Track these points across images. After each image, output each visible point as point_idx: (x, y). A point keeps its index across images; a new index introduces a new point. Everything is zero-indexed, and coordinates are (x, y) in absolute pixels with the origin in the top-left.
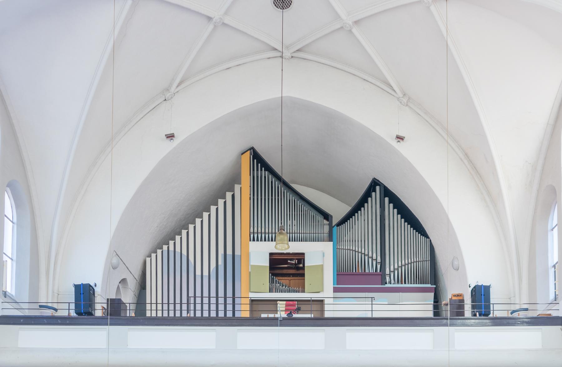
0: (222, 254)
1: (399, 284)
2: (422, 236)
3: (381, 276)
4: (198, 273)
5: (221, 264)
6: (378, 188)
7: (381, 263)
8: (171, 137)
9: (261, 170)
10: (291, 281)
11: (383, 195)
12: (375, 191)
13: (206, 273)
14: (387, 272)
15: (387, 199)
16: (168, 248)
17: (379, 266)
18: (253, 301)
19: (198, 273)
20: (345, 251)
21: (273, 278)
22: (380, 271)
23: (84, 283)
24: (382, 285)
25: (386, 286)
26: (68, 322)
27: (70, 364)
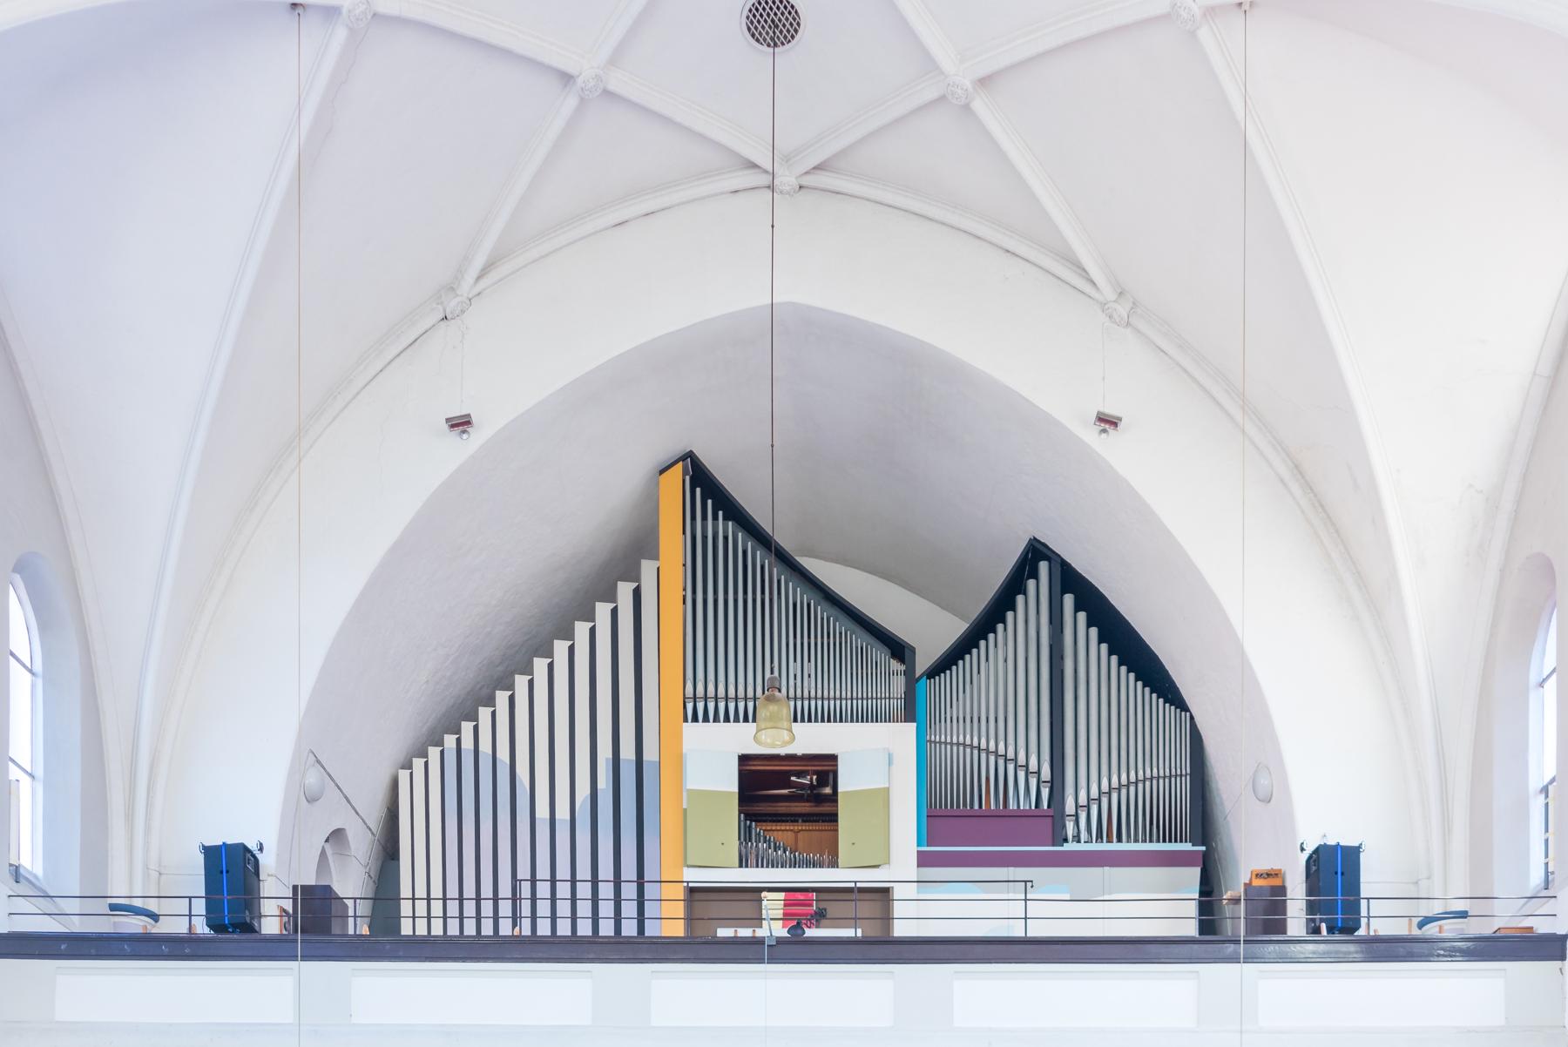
0: (607, 759)
1: (1102, 842)
2: (1167, 705)
3: (1051, 821)
4: (542, 812)
6: (1043, 567)
7: (1052, 784)
9: (715, 518)
10: (800, 835)
11: (1057, 588)
12: (1035, 575)
14: (1070, 807)
15: (1069, 600)
16: (459, 741)
17: (1045, 792)
18: (693, 892)
19: (542, 812)
21: (750, 827)
22: (1049, 806)
24: (1053, 845)
25: (1070, 846)
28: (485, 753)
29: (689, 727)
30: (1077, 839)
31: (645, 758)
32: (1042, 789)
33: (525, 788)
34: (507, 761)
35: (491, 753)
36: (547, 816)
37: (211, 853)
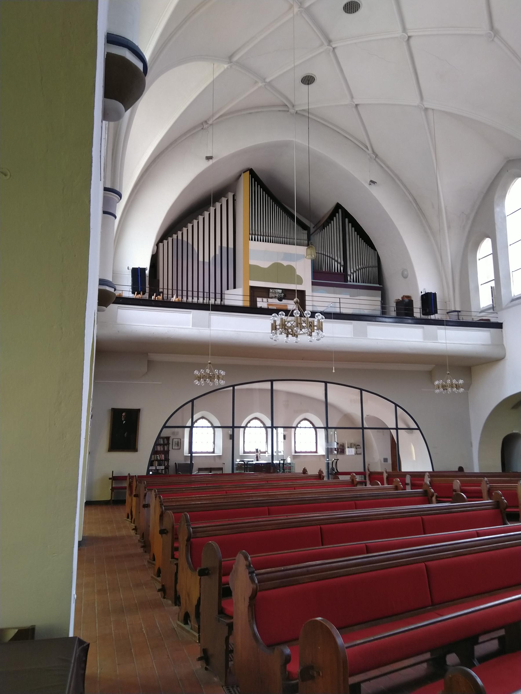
0: (219, 246)
2: (372, 249)
3: (343, 276)
4: (201, 259)
5: (218, 254)
6: (340, 210)
7: (344, 266)
8: (209, 158)
9: (258, 187)
13: (206, 260)
14: (349, 273)
15: (347, 220)
16: (177, 236)
18: (252, 288)
19: (201, 259)
20: (370, 268)
22: (343, 272)
23: (140, 267)
24: (345, 282)
25: (349, 283)
26: (160, 304)
27: (162, 339)
28: (224, 247)
29: (250, 241)
30: (350, 282)
31: (223, 245)
32: (341, 267)
33: (196, 252)
34: (191, 244)
35: (226, 246)
36: (202, 260)
37: (502, 323)
